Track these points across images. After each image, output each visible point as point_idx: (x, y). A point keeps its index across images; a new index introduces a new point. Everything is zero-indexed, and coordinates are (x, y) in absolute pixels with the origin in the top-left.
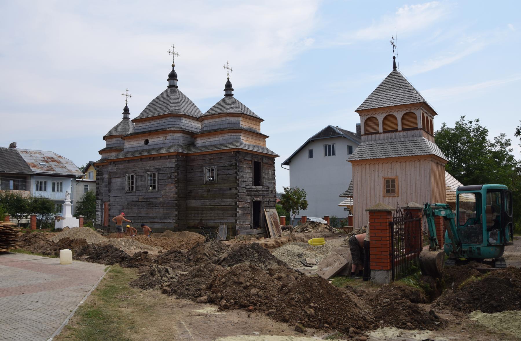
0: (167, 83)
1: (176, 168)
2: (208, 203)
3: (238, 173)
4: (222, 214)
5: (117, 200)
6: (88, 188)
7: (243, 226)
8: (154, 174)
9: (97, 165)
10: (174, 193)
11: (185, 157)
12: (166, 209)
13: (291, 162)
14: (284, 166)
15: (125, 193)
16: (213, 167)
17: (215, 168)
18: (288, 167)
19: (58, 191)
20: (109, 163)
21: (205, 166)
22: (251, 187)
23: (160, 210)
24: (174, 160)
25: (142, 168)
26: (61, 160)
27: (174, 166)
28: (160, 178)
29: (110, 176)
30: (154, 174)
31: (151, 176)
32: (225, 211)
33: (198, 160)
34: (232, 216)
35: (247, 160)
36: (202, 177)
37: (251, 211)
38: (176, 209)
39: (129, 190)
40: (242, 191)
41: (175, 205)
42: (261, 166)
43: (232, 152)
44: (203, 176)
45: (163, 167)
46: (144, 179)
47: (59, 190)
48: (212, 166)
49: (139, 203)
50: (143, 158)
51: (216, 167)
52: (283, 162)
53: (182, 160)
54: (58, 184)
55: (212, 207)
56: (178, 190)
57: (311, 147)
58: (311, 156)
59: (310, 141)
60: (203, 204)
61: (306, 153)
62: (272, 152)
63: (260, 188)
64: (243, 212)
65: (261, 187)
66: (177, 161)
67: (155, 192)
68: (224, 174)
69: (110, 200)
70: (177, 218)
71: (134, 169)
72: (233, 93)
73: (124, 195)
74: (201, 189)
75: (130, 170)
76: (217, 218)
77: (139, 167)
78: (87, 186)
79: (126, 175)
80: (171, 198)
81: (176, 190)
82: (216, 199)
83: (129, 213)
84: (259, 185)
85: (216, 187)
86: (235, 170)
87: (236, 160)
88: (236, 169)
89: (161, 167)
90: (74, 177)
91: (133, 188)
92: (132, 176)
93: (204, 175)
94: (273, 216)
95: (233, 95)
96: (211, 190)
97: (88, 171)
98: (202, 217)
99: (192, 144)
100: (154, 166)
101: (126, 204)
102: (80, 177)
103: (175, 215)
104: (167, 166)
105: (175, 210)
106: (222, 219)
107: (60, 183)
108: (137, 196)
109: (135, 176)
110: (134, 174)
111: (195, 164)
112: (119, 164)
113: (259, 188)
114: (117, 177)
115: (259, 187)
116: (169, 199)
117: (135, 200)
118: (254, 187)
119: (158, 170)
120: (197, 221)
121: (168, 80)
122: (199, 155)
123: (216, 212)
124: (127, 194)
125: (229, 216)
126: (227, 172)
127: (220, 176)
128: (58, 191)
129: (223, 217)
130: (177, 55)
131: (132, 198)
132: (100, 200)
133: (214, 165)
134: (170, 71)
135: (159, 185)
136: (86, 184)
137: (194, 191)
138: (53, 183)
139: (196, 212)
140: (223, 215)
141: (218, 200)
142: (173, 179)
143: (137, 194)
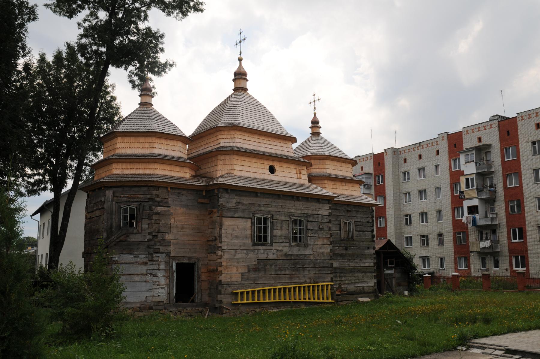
0: (232, 85)
10: (329, 250)
12: (319, 271)
23: (311, 272)
24: (327, 206)
34: (372, 279)
45: (313, 212)
49: (278, 262)
67: (302, 246)
72: (321, 131)
75: (263, 209)
76: (357, 281)
79: (256, 215)
85: (355, 244)
89: (310, 213)
92: (265, 219)
95: (321, 133)
100: (301, 210)
103: (330, 279)
105: (329, 272)
119: (308, 216)
121: (234, 80)
123: (356, 275)
129: (363, 280)
134: (235, 69)
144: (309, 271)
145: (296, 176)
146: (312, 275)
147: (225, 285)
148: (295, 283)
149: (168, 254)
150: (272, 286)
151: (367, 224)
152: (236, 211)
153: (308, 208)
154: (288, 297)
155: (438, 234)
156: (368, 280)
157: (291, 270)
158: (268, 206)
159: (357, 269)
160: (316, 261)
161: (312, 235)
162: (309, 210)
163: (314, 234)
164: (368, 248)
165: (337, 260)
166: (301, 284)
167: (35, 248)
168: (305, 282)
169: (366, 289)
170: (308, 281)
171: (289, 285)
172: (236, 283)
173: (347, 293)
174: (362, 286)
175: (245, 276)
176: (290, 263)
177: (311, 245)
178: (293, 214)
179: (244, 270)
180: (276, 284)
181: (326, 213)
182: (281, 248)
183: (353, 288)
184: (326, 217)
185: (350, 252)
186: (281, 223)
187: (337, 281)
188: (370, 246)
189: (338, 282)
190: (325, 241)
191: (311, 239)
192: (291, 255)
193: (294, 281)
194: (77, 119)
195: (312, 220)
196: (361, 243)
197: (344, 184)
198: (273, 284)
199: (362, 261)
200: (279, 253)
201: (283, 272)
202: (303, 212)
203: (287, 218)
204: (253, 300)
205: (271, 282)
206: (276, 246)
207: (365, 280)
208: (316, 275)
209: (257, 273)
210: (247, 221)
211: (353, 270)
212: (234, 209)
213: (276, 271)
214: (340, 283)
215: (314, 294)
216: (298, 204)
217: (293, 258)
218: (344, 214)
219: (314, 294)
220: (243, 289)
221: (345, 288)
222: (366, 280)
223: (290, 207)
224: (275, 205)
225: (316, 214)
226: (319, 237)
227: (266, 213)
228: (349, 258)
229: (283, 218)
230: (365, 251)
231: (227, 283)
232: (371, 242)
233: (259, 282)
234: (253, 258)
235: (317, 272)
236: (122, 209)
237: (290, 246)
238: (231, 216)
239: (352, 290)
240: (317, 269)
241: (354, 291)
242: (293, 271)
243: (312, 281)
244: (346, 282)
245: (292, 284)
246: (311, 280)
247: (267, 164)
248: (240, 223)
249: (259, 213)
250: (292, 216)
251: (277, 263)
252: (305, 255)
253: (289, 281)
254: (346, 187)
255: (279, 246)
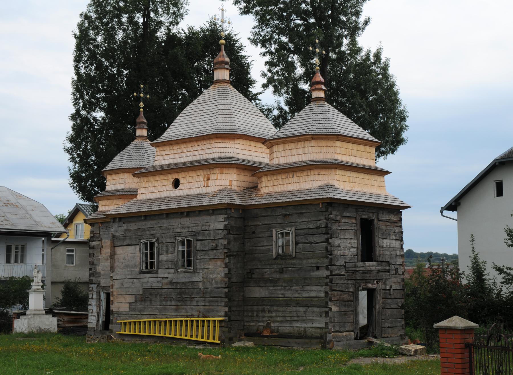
1: (226, 232)
2: (280, 293)
3: (330, 241)
4: (304, 312)
5: (126, 285)
6: (72, 255)
7: (340, 334)
8: (188, 241)
9: (92, 222)
10: (223, 275)
11: (241, 212)
12: (209, 302)
13: (459, 204)
14: (446, 213)
15: (140, 273)
16: (288, 230)
17: (292, 230)
18: (454, 214)
19: (16, 262)
20: (112, 220)
21: (275, 228)
22: (355, 265)
24: (221, 218)
25: (168, 229)
26: (22, 202)
27: (223, 228)
28: (198, 248)
29: (113, 242)
30: (188, 241)
31: (183, 245)
32: (308, 307)
33: (263, 216)
35: (348, 217)
36: (270, 245)
38: (226, 302)
39: (147, 268)
40: (337, 272)
41: (223, 296)
42: (374, 225)
43: (319, 204)
44: (272, 245)
45: (203, 228)
46: (171, 249)
47: (19, 260)
48: (288, 227)
49: (164, 291)
50: (171, 213)
51: (293, 229)
53: (236, 216)
54: (17, 248)
55: (287, 300)
56: (230, 270)
57: (498, 176)
58: (500, 193)
59: (497, 164)
60: (272, 294)
61: (491, 188)
62: (397, 199)
63: (373, 266)
64: (340, 309)
65: (374, 263)
66: (226, 219)
67: (190, 272)
68: (307, 241)
69: (113, 285)
70: (227, 318)
71: (155, 232)
73: (138, 276)
74: (268, 267)
75: (148, 233)
76: (296, 318)
77: (163, 228)
78: (72, 251)
79: (142, 241)
80: (216, 283)
81: (226, 269)
83: (145, 308)
84: (371, 260)
85: (294, 264)
86: (326, 236)
87: (327, 219)
88: (327, 233)
89: (200, 230)
90: (47, 235)
91: (152, 264)
92: (152, 244)
93: (274, 244)
96: (285, 269)
97: (74, 222)
98: (271, 317)
99: (254, 188)
100: (189, 228)
101: (141, 292)
102: (59, 234)
103: (223, 314)
104: (211, 228)
105: (223, 304)
106: (304, 320)
107: (20, 247)
108: (159, 279)
109: (156, 244)
110: (154, 240)
111: (258, 223)
112: (130, 222)
113: (371, 265)
114: (124, 244)
115: (371, 263)
116: (214, 286)
117: (155, 285)
118: (360, 264)
119: (196, 234)
120: (262, 324)
122: (264, 208)
124: (143, 276)
125: (315, 315)
126: (311, 239)
127: (300, 246)
128: (16, 262)
129: (305, 318)
130: (229, 23)
131: (152, 283)
132: (95, 284)
133: (291, 226)
135: (198, 261)
136: (70, 247)
137: (258, 270)
138: (7, 247)
139: (261, 308)
140: (305, 314)
141: (297, 287)
142: (221, 251)
143: (159, 275)
144: (197, 301)
145: (202, 184)
146: (201, 307)
147: (115, 315)
148: (182, 316)
149: (99, 285)
150: (157, 317)
151: (316, 230)
152: (125, 239)
154: (189, 334)
155: (7, 263)
156: (314, 318)
157: (177, 301)
159: (296, 300)
161: (202, 257)
162: (197, 226)
163: (204, 255)
164: (318, 268)
165: (266, 287)
166: (187, 317)
168: (192, 316)
169: (311, 332)
170: (196, 314)
171: (174, 318)
172: (124, 313)
173: (278, 335)
174: (303, 326)
175: (133, 306)
176: (176, 292)
177: (200, 269)
178: (179, 234)
179: (131, 299)
180: (161, 316)
181: (221, 226)
182: (166, 275)
183: (288, 328)
184: (220, 232)
185: (286, 276)
186: (167, 246)
187: (264, 317)
188: (319, 265)
189: (266, 319)
190: (219, 263)
191: (200, 262)
192: (177, 283)
193: (181, 314)
196: (304, 261)
197: (291, 175)
198: (158, 316)
199: (305, 289)
200: (165, 281)
201: (169, 303)
203: (173, 240)
204: (140, 332)
205: (157, 314)
206: (162, 273)
207: (308, 318)
208: (207, 307)
209: (143, 303)
210: (136, 248)
211: (288, 302)
212: (122, 238)
213: (161, 301)
214: (269, 320)
215: (181, 330)
216: (186, 221)
217: (179, 286)
218: (279, 221)
219: (181, 330)
220: (131, 319)
221: (276, 328)
222: (311, 318)
223: (175, 227)
224: (159, 227)
225: (206, 230)
226: (210, 259)
227: (151, 237)
228: (284, 284)
229: (169, 240)
230: (312, 274)
231: (117, 313)
232: (322, 259)
233: (145, 313)
234: (138, 287)
235: (207, 304)
237: (176, 272)
238: (120, 245)
239: (287, 331)
240: (207, 299)
241: (290, 333)
242: (179, 301)
243: (201, 315)
244: (279, 319)
245: (178, 316)
246: (200, 313)
247: (171, 178)
248: (130, 250)
249: (145, 238)
250: (179, 237)
251: (161, 292)
252: (192, 283)
253: (176, 314)
254: (295, 180)
255: (164, 273)
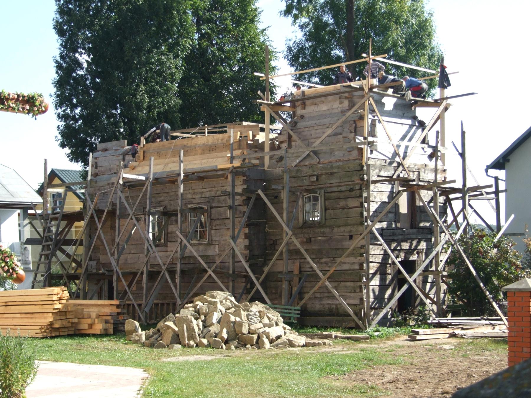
13: (508, 161)
37: (283, 267)
52: (490, 160)
76: (326, 295)
82: (322, 258)
85: (323, 233)
94: (500, 296)
153: (211, 189)
158: (159, 195)
160: (223, 264)
167: (392, 248)
174: (334, 303)
177: (216, 241)
178: (190, 200)
194: (121, 120)
195: (217, 205)
202: (203, 196)
236: (305, 197)
